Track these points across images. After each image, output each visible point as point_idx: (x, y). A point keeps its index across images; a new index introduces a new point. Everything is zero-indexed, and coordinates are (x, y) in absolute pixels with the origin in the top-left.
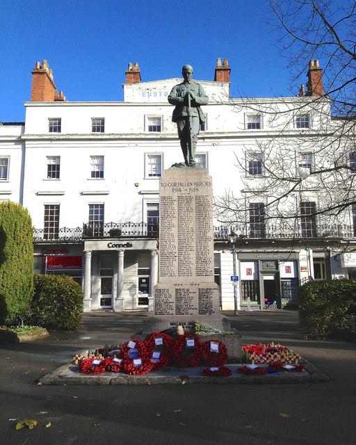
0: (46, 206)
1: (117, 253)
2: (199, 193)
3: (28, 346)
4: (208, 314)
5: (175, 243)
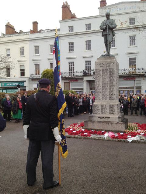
0: (69, 63)
2: (111, 67)
4: (113, 114)
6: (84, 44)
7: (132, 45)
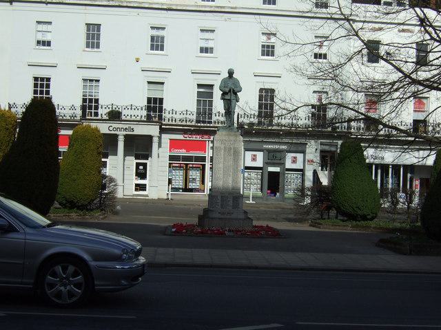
0: (36, 79)
1: (117, 136)
3: (230, 236)
6: (83, 31)
7: (158, 50)
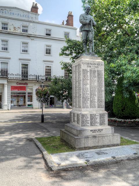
2: (99, 69)
5: (88, 92)
